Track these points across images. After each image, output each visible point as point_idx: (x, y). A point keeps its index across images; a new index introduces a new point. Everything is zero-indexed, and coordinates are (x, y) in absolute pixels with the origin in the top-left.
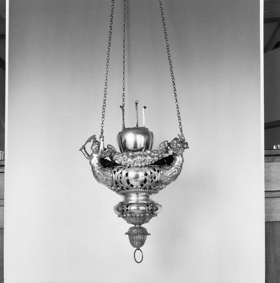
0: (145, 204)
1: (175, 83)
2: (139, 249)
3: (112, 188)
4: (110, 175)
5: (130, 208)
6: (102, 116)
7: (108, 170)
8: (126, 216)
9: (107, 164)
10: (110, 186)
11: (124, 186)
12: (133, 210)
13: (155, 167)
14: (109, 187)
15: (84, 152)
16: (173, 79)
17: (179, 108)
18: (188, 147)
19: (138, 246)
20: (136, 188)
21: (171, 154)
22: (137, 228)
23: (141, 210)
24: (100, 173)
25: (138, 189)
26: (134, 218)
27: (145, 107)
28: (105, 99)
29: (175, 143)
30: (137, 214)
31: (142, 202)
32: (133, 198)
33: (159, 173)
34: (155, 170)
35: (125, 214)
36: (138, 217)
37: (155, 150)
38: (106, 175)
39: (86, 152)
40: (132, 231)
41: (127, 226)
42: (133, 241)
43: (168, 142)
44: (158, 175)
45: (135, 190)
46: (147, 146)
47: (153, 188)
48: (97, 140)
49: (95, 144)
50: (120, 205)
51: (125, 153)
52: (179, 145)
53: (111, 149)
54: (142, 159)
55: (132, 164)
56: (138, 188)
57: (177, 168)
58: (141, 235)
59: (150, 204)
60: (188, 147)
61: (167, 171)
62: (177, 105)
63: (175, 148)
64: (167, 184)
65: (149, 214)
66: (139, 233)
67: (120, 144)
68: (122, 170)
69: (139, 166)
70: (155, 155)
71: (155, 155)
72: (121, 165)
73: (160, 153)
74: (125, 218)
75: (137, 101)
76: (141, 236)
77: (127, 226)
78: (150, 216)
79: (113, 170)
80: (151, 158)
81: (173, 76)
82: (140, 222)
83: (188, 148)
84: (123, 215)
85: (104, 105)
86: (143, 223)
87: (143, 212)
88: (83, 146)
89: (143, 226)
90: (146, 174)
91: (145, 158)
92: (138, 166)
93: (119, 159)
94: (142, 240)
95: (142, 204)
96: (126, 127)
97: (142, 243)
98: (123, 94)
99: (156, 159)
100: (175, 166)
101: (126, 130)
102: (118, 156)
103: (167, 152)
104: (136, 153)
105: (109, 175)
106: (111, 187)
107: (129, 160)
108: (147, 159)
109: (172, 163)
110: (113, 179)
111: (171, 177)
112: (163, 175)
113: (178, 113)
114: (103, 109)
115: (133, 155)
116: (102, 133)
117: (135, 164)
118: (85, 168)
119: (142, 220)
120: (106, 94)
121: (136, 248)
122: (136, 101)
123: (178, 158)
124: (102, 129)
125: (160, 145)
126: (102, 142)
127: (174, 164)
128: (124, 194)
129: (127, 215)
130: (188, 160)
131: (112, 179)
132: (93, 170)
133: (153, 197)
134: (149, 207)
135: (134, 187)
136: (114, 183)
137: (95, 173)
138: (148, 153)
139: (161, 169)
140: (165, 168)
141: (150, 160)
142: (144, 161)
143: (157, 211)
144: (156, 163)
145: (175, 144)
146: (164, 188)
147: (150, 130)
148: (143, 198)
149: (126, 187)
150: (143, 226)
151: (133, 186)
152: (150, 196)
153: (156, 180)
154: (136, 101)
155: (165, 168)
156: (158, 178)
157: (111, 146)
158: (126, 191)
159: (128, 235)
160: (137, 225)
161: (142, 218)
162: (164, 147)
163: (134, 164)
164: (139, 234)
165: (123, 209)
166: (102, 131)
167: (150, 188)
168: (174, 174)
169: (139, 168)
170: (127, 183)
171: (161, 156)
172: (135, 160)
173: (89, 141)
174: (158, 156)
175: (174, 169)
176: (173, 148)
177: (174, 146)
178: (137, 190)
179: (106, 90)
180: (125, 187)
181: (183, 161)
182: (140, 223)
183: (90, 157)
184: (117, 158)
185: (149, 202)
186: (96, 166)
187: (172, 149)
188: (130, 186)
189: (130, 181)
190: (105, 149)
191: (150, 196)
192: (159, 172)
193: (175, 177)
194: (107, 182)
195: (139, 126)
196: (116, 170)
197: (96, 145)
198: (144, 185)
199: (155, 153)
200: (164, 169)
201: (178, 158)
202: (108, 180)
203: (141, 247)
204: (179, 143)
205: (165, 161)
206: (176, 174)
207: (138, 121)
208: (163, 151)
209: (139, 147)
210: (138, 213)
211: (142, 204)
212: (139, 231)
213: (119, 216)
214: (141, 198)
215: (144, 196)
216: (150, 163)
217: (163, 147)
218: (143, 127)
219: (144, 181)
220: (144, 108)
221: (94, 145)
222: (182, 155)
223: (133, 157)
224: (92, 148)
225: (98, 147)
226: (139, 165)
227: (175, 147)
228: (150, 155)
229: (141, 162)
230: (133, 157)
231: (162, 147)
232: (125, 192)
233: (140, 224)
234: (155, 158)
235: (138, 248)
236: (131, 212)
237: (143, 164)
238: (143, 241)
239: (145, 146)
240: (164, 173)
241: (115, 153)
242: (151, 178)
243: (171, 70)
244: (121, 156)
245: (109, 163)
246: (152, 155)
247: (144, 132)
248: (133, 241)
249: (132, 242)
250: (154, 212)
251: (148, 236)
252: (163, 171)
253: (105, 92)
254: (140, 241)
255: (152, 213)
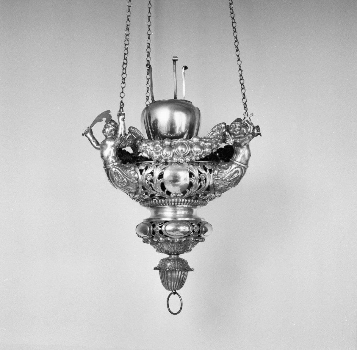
0: (189, 222)
1: (236, 29)
2: (175, 293)
3: (136, 196)
4: (134, 175)
5: (165, 228)
6: (121, 80)
7: (131, 167)
8: (158, 241)
9: (128, 157)
10: (133, 193)
11: (156, 194)
12: (170, 231)
13: (205, 163)
14: (130, 195)
15: (91, 138)
16: (233, 23)
17: (242, 71)
18: (260, 134)
19: (174, 288)
20: (174, 197)
21: (231, 144)
22: (174, 260)
23: (182, 232)
24: (117, 173)
25: (178, 199)
26: (171, 244)
27: (186, 68)
28: (126, 52)
29: (238, 127)
30: (175, 237)
31: (183, 219)
32: (168, 213)
33: (212, 173)
34: (205, 169)
35: (157, 237)
36: (177, 243)
37: (205, 138)
38: (127, 175)
39: (94, 138)
40: (165, 265)
41: (157, 257)
42: (167, 281)
43: (226, 125)
44: (210, 176)
45: (173, 200)
46: (191, 130)
47: (201, 197)
48: (112, 119)
49: (110, 125)
50: (149, 223)
51: (158, 141)
52: (244, 130)
53: (135, 134)
54: (186, 150)
55: (170, 159)
56: (179, 197)
57: (240, 167)
58: (180, 271)
59: (195, 222)
60: (260, 134)
61: (225, 171)
62: (240, 66)
63: (238, 134)
64: (222, 191)
65: (195, 238)
66: (178, 267)
67: (148, 125)
68: (154, 168)
69: (180, 162)
70: (206, 146)
71: (207, 145)
72: (151, 160)
73: (214, 142)
74: (154, 244)
75: (176, 57)
76: (180, 272)
77: (157, 257)
78: (196, 240)
79: (138, 168)
80: (200, 150)
81: (233, 18)
82: (179, 251)
83: (261, 136)
84: (153, 239)
85: (125, 61)
86: (183, 253)
87: (185, 234)
88: (88, 128)
89: (182, 256)
90: (191, 175)
91: (190, 149)
92: (178, 163)
93: (148, 149)
94: (181, 279)
95: (183, 223)
96: (156, 100)
97: (181, 283)
98: (148, 44)
99: (208, 151)
100: (236, 162)
101: (156, 104)
102: (147, 145)
103: (224, 141)
104: (176, 141)
105: (133, 175)
106: (134, 195)
107: (165, 152)
108: (194, 151)
109: (231, 158)
110: (138, 183)
111: (230, 181)
112: (218, 177)
113: (241, 79)
114: (124, 69)
115: (171, 144)
116: (121, 108)
117: (174, 159)
118: (91, 164)
119: (182, 248)
120: (128, 45)
121: (171, 292)
122: (174, 57)
123: (241, 150)
124: (122, 102)
125: (213, 129)
126: (122, 122)
127: (235, 160)
128: (152, 206)
129: (159, 239)
130: (256, 154)
131: (136, 182)
132: (106, 167)
133: (199, 212)
134: (195, 227)
135: (172, 196)
136: (140, 188)
137: (110, 173)
138: (194, 141)
139: (214, 167)
140: (220, 166)
141: (199, 152)
142: (188, 155)
143: (206, 234)
144: (206, 159)
145: (237, 128)
146: (216, 198)
147: (195, 104)
148: (183, 212)
149: (158, 195)
150: (182, 256)
151: (171, 193)
152: (195, 210)
153: (207, 184)
154: (174, 57)
155: (220, 166)
156: (210, 181)
157: (136, 129)
158: (159, 201)
159: (158, 271)
160: (173, 256)
161: (182, 245)
162: (219, 132)
163: (173, 159)
164: (178, 269)
165: (153, 229)
166: (122, 104)
167: (196, 196)
168: (236, 175)
169: (180, 165)
170: (160, 189)
171: (216, 147)
172: (175, 153)
173: (98, 119)
174: (210, 147)
175: (236, 168)
176: (234, 135)
177: (236, 132)
178: (176, 200)
179: (128, 37)
180: (157, 195)
181: (250, 156)
182: (180, 252)
183: (101, 146)
184: (145, 147)
185: (193, 219)
186: (111, 159)
187: (233, 137)
188: (165, 193)
189: (166, 186)
190: (126, 135)
191: (195, 210)
192: (212, 171)
193: (236, 181)
194: (129, 187)
195: (179, 98)
196: (143, 167)
197: (111, 127)
198: (188, 193)
199: (206, 142)
200: (220, 167)
201: (241, 150)
202: (131, 184)
203: (178, 289)
204: (244, 127)
205: (218, 155)
206: (239, 175)
207: (176, 89)
208: (219, 139)
209: (177, 132)
210: (178, 237)
211: (183, 223)
212: (177, 264)
213: (145, 241)
214: (181, 213)
215: (185, 209)
216: (198, 158)
217: (218, 132)
218: (182, 99)
219: (188, 185)
220: (184, 68)
221: (109, 127)
222: (248, 146)
223: (172, 147)
224: (104, 131)
225: (114, 130)
226: (181, 160)
227: (238, 133)
228: (198, 144)
229: (184, 156)
230: (171, 147)
231: (216, 133)
232: (157, 203)
233: (178, 254)
234: (207, 150)
235: (174, 291)
236: (166, 234)
237: (187, 159)
238: (182, 281)
239: (187, 131)
240: (219, 173)
241: (142, 140)
242: (200, 180)
243: (231, 7)
244: (152, 145)
245: (128, 157)
246: (201, 144)
247: (186, 107)
248: (167, 281)
249: (166, 281)
250: (202, 236)
251: (189, 272)
252: (218, 170)
253: (127, 41)
254: (179, 279)
255: (199, 236)
